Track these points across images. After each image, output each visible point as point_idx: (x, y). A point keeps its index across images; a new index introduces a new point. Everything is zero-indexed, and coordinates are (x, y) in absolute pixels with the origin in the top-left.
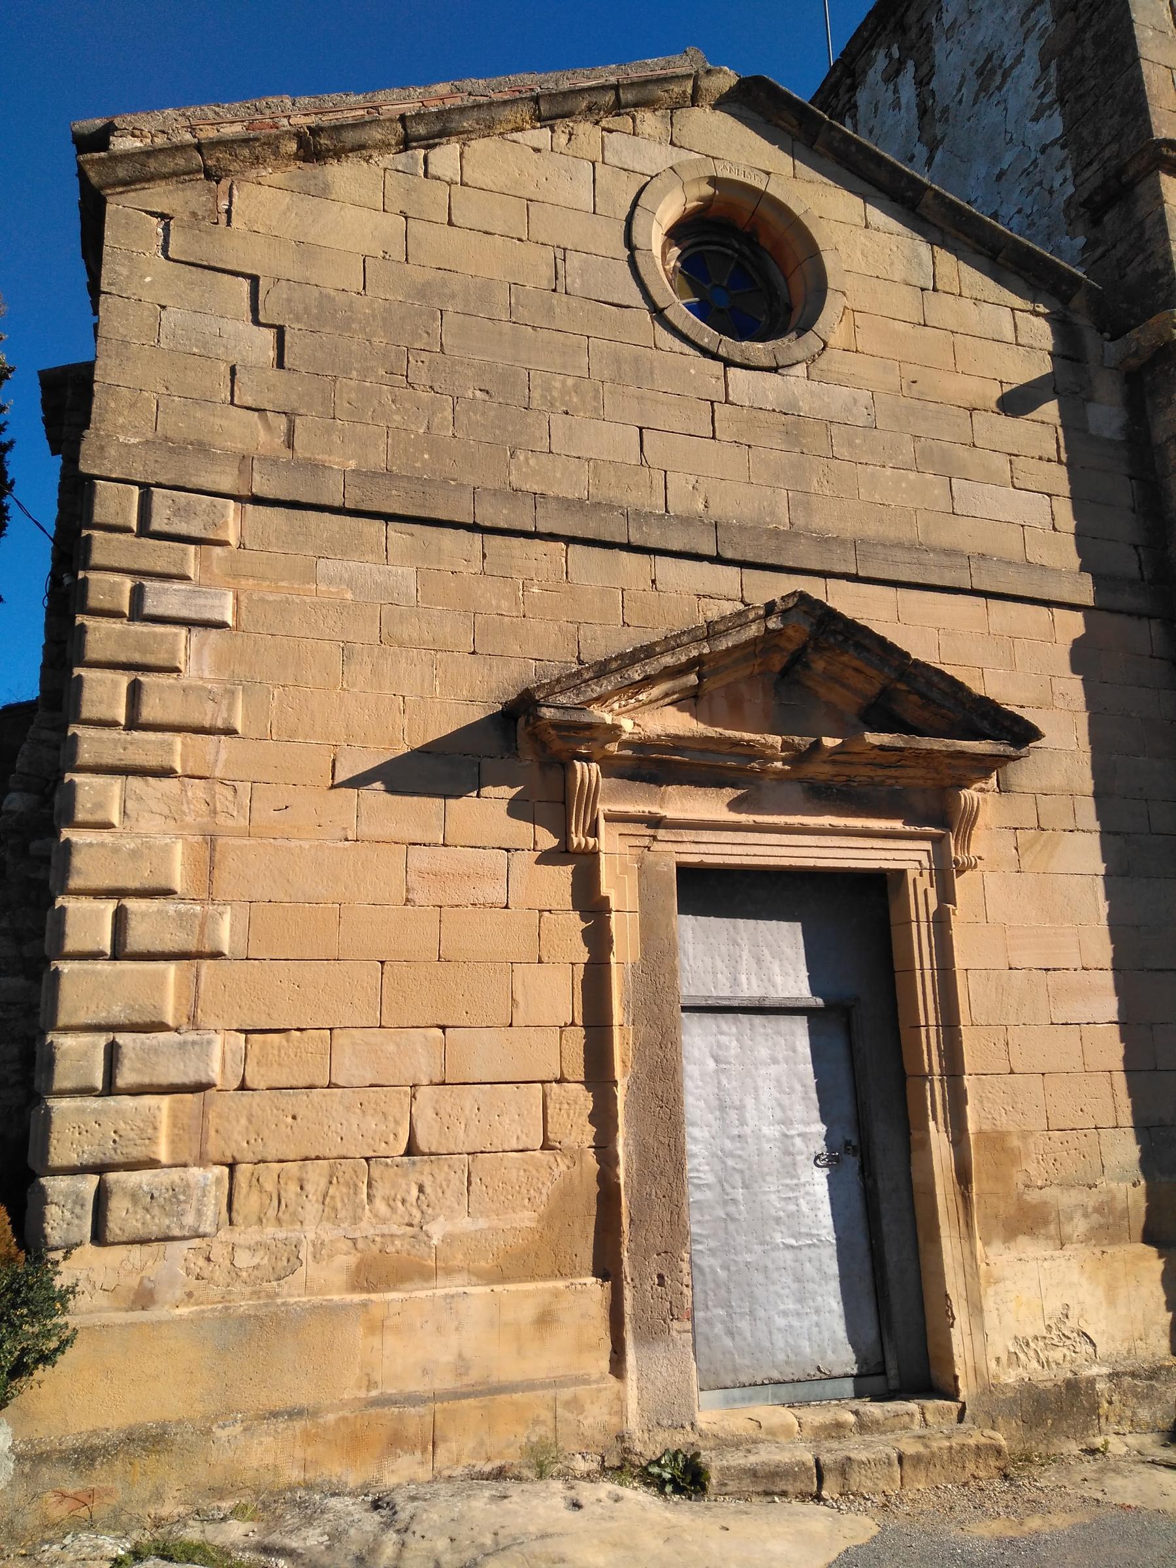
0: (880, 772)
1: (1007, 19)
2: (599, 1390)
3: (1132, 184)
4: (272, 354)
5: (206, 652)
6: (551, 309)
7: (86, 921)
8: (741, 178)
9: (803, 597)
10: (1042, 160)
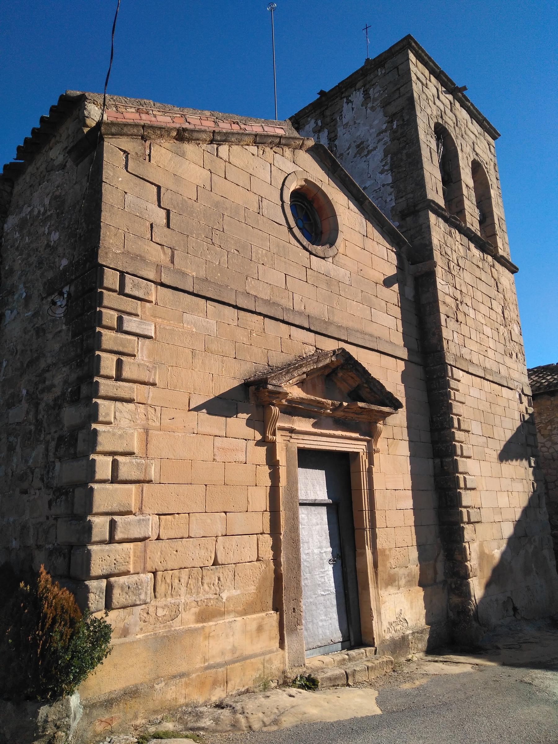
0: (356, 416)
1: (371, 131)
2: (277, 655)
3: (418, 211)
4: (165, 221)
5: (145, 348)
6: (258, 221)
7: (103, 466)
8: (314, 181)
9: (343, 350)
10: (382, 189)
